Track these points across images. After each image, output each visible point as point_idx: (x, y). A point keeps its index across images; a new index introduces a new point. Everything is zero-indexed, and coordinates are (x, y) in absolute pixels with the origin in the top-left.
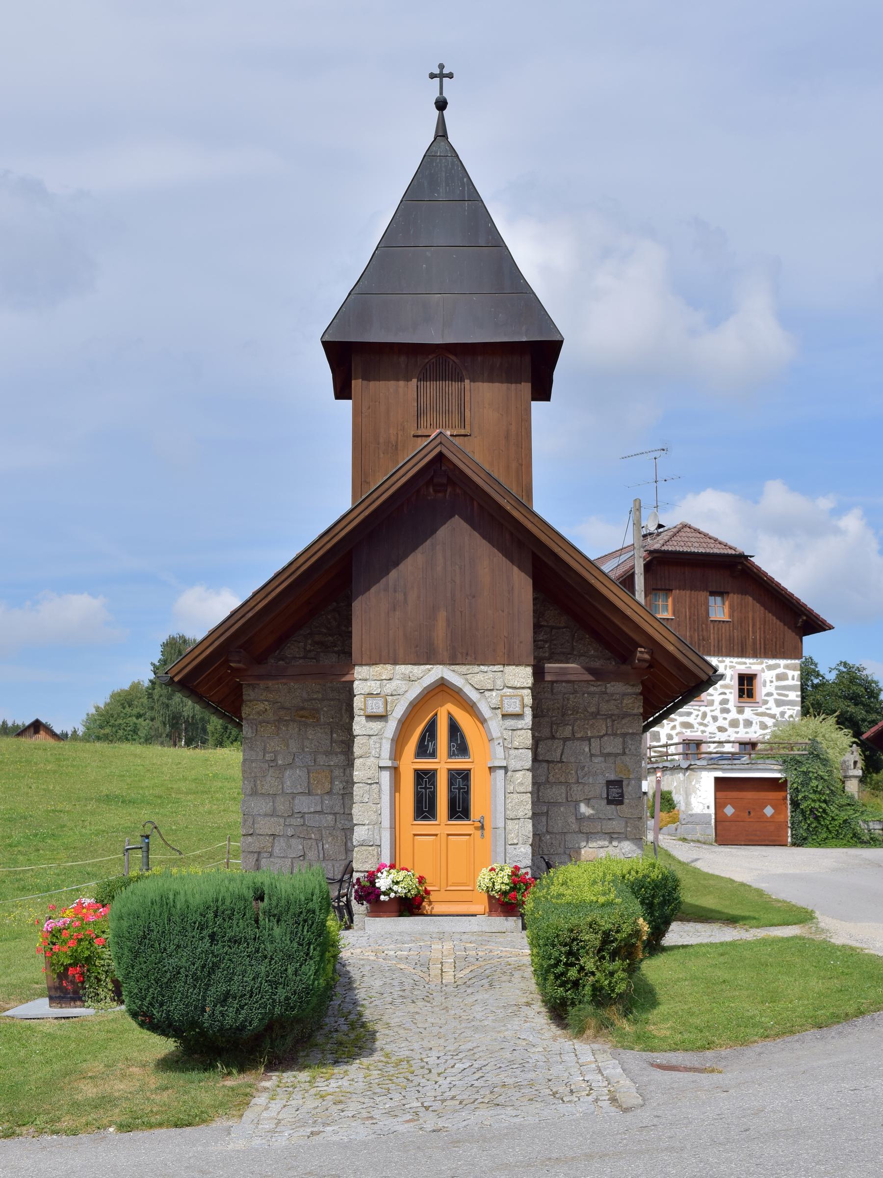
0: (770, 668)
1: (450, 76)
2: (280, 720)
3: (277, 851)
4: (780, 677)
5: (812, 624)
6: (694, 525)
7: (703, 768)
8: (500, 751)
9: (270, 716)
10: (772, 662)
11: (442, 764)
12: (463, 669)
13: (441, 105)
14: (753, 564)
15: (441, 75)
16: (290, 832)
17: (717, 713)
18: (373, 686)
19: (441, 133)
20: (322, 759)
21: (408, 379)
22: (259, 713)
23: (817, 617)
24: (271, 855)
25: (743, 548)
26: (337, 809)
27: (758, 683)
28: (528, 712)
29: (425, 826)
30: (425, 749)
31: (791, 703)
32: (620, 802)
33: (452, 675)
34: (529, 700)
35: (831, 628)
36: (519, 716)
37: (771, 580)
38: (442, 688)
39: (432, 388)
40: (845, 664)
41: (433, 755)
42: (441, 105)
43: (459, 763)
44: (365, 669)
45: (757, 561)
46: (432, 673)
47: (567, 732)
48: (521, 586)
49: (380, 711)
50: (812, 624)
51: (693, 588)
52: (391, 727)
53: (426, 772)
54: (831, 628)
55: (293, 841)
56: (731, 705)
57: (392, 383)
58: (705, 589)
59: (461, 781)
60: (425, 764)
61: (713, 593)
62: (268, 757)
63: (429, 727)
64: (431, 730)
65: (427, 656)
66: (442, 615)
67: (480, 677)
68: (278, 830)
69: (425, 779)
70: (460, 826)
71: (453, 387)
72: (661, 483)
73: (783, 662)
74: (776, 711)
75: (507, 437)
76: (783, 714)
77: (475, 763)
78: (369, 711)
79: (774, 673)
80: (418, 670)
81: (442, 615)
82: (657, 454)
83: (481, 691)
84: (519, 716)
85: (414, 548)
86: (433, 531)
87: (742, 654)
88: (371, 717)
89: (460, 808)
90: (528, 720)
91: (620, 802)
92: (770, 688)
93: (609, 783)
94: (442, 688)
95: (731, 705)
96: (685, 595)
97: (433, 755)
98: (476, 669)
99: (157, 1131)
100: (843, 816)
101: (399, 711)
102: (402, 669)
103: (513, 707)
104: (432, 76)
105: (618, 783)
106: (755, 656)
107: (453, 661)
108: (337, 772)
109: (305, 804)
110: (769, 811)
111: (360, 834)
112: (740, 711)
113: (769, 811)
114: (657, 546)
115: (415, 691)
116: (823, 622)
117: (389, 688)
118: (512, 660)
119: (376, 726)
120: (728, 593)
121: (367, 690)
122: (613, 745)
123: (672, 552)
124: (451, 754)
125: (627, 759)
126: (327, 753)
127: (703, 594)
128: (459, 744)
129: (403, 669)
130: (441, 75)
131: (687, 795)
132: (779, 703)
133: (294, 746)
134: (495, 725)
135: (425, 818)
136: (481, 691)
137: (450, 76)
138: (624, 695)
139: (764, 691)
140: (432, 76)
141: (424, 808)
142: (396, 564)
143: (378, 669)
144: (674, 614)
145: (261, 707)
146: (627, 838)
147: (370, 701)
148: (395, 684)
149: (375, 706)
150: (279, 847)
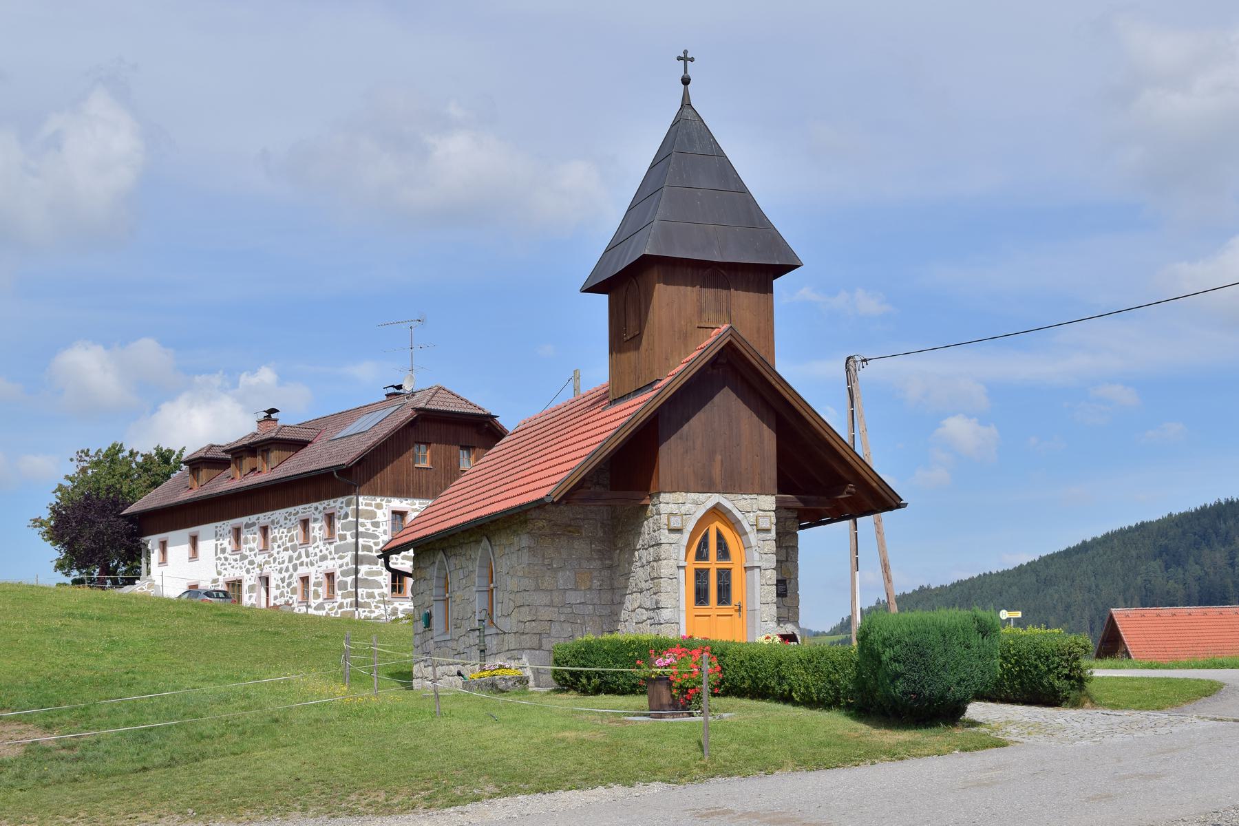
1: (692, 60)
2: (554, 534)
3: (553, 632)
6: (447, 388)
8: (756, 555)
9: (547, 531)
11: (713, 564)
12: (732, 496)
13: (686, 81)
14: (497, 423)
16: (562, 618)
19: (686, 103)
20: (585, 564)
21: (693, 286)
22: (539, 529)
24: (549, 635)
25: (490, 409)
26: (596, 601)
28: (774, 528)
29: (702, 610)
30: (701, 555)
32: (785, 596)
36: (768, 531)
38: (717, 512)
39: (710, 293)
41: (706, 558)
42: (686, 81)
43: (724, 565)
46: (713, 499)
48: (769, 439)
49: (679, 526)
51: (446, 443)
52: (686, 536)
53: (702, 570)
55: (565, 625)
57: (682, 288)
58: (455, 443)
59: (724, 576)
60: (702, 565)
61: (463, 448)
62: (546, 562)
63: (710, 541)
64: (704, 543)
65: (709, 488)
66: (718, 458)
67: (742, 502)
68: (555, 617)
69: (701, 575)
70: (725, 610)
71: (723, 293)
72: (416, 349)
75: (758, 331)
77: (735, 564)
78: (672, 526)
80: (702, 497)
81: (718, 458)
82: (411, 324)
84: (768, 531)
85: (699, 409)
86: (712, 397)
88: (672, 531)
89: (724, 595)
90: (773, 533)
91: (785, 596)
96: (442, 447)
97: (706, 558)
98: (740, 496)
99: (989, 750)
101: (690, 526)
103: (764, 524)
104: (679, 58)
107: (725, 491)
108: (595, 573)
109: (573, 597)
114: (422, 405)
115: (700, 512)
117: (684, 509)
119: (675, 536)
120: (474, 447)
121: (669, 511)
123: (434, 411)
124: (719, 558)
125: (789, 564)
126: (589, 559)
127: (454, 449)
128: (724, 552)
129: (693, 496)
130: (685, 59)
133: (564, 555)
134: (753, 537)
135: (702, 604)
137: (692, 60)
138: (786, 518)
140: (679, 58)
141: (701, 597)
142: (688, 420)
143: (677, 495)
144: (432, 463)
145: (540, 524)
146: (789, 621)
147: (673, 519)
148: (688, 506)
149: (676, 522)
150: (555, 629)
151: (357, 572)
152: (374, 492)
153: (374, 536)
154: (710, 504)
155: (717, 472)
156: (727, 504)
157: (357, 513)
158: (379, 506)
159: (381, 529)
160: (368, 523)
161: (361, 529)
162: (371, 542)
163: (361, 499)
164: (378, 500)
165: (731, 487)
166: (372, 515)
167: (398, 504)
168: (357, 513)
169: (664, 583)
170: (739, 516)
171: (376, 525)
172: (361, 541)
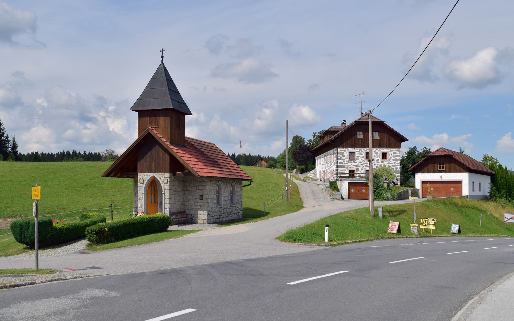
0: (391, 151)
4: (394, 153)
5: (404, 139)
7: (345, 180)
10: (392, 149)
13: (162, 57)
15: (162, 51)
17: (376, 163)
18: (141, 177)
23: (404, 137)
27: (388, 155)
31: (397, 160)
33: (155, 175)
34: (169, 180)
35: (408, 140)
36: (167, 183)
37: (390, 128)
40: (426, 148)
42: (162, 57)
44: (143, 174)
45: (386, 123)
47: (192, 185)
50: (404, 139)
54: (408, 140)
56: (380, 161)
63: (154, 185)
65: (150, 171)
73: (395, 149)
74: (393, 162)
76: (395, 163)
79: (392, 152)
83: (161, 178)
87: (383, 147)
88: (141, 183)
92: (391, 156)
93: (200, 195)
94: (154, 177)
95: (380, 161)
100: (381, 192)
102: (146, 174)
105: (202, 195)
106: (387, 148)
107: (155, 172)
110: (364, 191)
111: (139, 206)
112: (382, 162)
113: (364, 191)
116: (406, 138)
117: (144, 177)
118: (166, 172)
119: (142, 185)
122: (201, 188)
131: (341, 187)
132: (394, 160)
136: (161, 178)
139: (390, 157)
151: (337, 170)
152: (343, 147)
153: (343, 159)
154: (151, 176)
155: (153, 167)
156: (156, 176)
157: (337, 153)
158: (345, 151)
159: (346, 157)
160: (341, 156)
161: (339, 158)
162: (342, 161)
163: (339, 149)
164: (345, 149)
165: (158, 170)
166: (342, 153)
167: (351, 150)
168: (337, 153)
169: (139, 197)
170: (159, 179)
171: (344, 156)
172: (339, 161)
